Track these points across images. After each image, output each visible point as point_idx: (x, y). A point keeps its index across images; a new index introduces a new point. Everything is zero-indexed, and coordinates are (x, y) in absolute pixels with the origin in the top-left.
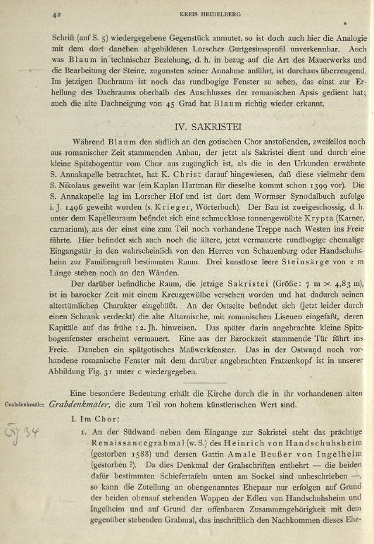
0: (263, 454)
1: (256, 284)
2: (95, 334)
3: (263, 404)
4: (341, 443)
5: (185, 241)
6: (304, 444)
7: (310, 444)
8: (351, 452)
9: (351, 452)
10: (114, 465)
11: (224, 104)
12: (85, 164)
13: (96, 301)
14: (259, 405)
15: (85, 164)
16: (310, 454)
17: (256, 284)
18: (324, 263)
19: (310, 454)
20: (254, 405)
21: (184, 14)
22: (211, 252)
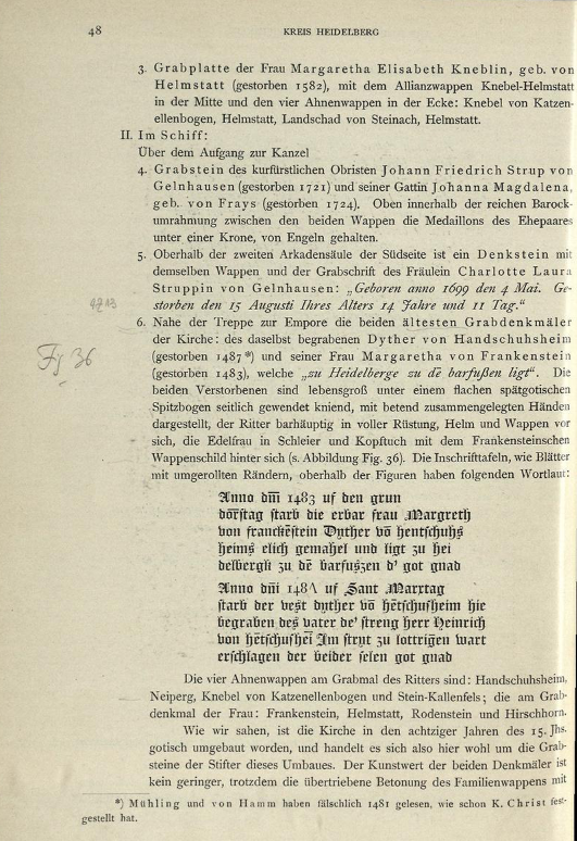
0: (368, 357)
1: (435, 323)
2: (213, 418)
3: (526, 473)
4: (540, 340)
5: (206, 255)
6: (482, 340)
7: (492, 341)
8: (556, 337)
9: (556, 337)
10: (187, 358)
11: (203, 69)
12: (171, 408)
13: (417, 724)
14: (518, 474)
15: (171, 408)
16: (443, 340)
17: (435, 323)
18: (160, 205)
19: (443, 340)
20: (511, 475)
21: (289, 31)
22: (450, 426)
